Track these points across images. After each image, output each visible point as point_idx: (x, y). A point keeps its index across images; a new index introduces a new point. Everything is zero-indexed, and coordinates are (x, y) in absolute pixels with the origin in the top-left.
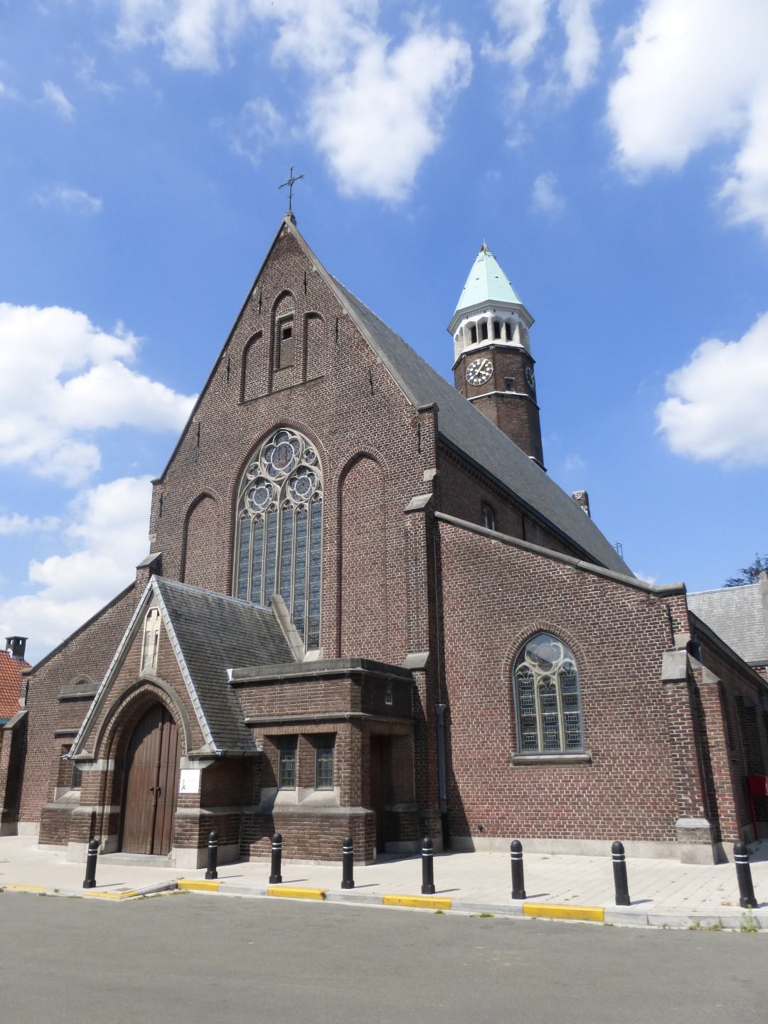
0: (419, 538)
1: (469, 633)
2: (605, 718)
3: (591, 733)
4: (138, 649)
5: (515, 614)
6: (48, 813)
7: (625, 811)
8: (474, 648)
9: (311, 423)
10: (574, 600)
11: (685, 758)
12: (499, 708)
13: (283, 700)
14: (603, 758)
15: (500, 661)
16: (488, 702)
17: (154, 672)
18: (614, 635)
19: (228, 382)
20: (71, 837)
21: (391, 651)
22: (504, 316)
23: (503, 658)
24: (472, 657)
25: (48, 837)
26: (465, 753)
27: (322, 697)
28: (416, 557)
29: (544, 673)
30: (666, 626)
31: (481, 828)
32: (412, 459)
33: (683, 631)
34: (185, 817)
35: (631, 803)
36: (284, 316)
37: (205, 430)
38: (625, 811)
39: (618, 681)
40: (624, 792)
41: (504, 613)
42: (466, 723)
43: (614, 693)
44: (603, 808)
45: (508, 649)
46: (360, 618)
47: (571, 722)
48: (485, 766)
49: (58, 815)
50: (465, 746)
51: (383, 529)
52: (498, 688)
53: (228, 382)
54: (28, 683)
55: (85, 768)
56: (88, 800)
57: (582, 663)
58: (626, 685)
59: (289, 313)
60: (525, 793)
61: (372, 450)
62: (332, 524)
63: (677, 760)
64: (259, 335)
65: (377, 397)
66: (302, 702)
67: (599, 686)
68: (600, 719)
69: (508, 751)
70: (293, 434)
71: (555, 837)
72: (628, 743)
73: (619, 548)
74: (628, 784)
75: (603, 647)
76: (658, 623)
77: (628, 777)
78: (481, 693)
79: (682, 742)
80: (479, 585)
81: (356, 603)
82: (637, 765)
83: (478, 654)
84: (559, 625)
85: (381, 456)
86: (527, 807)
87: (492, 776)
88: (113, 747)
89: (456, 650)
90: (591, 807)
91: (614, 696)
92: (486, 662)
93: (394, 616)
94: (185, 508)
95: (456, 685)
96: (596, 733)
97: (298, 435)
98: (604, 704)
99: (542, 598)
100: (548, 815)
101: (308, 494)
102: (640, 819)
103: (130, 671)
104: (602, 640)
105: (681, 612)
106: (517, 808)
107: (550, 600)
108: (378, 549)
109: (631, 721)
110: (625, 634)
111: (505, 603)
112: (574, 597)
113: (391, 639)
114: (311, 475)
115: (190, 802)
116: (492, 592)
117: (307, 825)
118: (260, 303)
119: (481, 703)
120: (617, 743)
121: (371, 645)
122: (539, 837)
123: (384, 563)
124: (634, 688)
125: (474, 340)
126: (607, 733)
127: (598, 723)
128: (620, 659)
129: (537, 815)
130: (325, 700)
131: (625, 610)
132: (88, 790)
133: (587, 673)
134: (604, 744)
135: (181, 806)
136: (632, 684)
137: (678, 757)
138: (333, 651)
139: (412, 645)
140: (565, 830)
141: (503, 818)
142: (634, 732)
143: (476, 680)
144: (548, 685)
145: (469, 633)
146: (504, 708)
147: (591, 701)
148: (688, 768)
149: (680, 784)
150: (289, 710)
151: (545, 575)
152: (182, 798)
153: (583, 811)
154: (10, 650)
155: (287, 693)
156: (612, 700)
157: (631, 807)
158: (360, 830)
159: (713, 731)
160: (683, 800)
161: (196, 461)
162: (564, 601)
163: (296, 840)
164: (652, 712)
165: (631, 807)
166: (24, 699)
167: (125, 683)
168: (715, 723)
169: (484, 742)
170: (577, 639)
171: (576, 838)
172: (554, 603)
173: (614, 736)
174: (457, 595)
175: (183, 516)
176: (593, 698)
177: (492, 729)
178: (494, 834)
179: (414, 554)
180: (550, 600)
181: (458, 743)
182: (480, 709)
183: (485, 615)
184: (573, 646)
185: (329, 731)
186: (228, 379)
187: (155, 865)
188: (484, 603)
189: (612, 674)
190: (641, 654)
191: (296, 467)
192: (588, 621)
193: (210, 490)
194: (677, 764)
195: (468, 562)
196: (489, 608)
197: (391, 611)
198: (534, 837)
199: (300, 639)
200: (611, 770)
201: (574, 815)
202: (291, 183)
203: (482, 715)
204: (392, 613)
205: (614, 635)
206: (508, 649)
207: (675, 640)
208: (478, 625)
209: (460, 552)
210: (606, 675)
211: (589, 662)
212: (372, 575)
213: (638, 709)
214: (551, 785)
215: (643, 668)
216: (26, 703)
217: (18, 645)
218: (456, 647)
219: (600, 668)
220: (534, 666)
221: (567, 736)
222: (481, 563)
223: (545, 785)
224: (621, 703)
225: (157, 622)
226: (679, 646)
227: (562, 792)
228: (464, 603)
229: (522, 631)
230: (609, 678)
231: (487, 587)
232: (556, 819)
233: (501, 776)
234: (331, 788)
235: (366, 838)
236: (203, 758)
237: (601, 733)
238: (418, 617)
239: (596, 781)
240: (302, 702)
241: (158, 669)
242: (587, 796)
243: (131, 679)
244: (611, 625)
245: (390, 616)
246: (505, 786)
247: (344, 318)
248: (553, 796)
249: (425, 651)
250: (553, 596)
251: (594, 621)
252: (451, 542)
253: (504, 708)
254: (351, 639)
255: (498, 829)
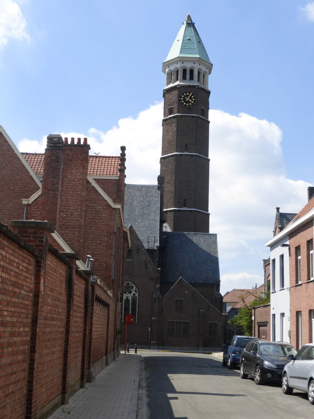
22: (188, 66)
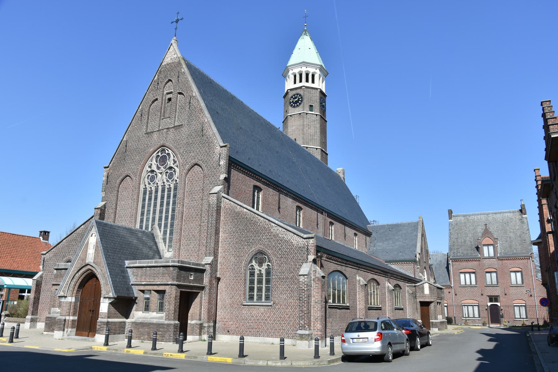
0: (214, 206)
1: (232, 249)
2: (279, 289)
3: (273, 295)
4: (86, 250)
5: (250, 243)
6: (48, 319)
7: (282, 326)
8: (233, 256)
9: (175, 147)
10: (273, 238)
11: (303, 306)
12: (240, 282)
13: (146, 275)
14: (277, 305)
15: (242, 262)
16: (236, 279)
17: (92, 261)
18: (286, 254)
19: (141, 122)
20: (56, 329)
21: (200, 255)
23: (243, 261)
24: (232, 260)
25: (49, 329)
26: (225, 300)
27: (161, 275)
28: (212, 214)
29: (259, 268)
30: (306, 252)
31: (228, 332)
32: (216, 169)
33: (312, 255)
34: (101, 322)
35: (285, 324)
36: (169, 91)
37: (129, 144)
38: (282, 326)
39: (286, 274)
40: (283, 319)
41: (246, 241)
42: (227, 288)
43: (284, 278)
44: (274, 325)
45: (246, 257)
46: (189, 239)
47: (268, 289)
48: (232, 306)
49: (53, 319)
50: (226, 297)
51: (202, 200)
52: (240, 274)
53: (141, 122)
54: (44, 259)
55: (63, 300)
56: (63, 314)
57: (273, 265)
58: (288, 275)
59: (171, 91)
60: (246, 318)
61: (200, 163)
62: (181, 195)
63: (301, 307)
64: (157, 99)
65: (205, 138)
66: (153, 277)
67: (278, 275)
68: (277, 289)
69: (242, 300)
70: (168, 151)
71: (256, 336)
72: (286, 299)
73: (358, 198)
74: (284, 316)
75: (282, 259)
76: (303, 250)
77: (285, 313)
78: (234, 275)
79: (303, 300)
80: (237, 229)
81: (188, 232)
82: (289, 308)
83: (234, 258)
84: (266, 248)
85: (203, 166)
86: (246, 324)
87: (235, 310)
88: (74, 292)
89: (226, 256)
90: (270, 324)
91: (283, 280)
92: (237, 262)
93: (203, 239)
94: (118, 181)
95: (224, 271)
96: (275, 295)
97: (170, 152)
98: (279, 283)
99: (261, 236)
100: (254, 327)
101: (172, 180)
102: (287, 330)
103: (83, 260)
104: (282, 256)
105: (312, 247)
106: (243, 324)
107: (264, 237)
108: (199, 209)
109: (288, 290)
110: (290, 254)
111: (247, 237)
112: (274, 237)
113: (200, 249)
114: (174, 171)
115: (103, 316)
116: (242, 232)
117: (151, 327)
118: (158, 84)
119: (234, 279)
120: (282, 299)
121: (193, 251)
122: (250, 336)
123: (201, 215)
124: (291, 277)
125: (295, 83)
126: (279, 295)
127: (276, 290)
128: (287, 265)
129: (250, 327)
130: (162, 277)
131: (292, 244)
132: (63, 309)
133: (275, 270)
134: (278, 299)
135: (100, 318)
136: (291, 275)
137: (301, 306)
138: (177, 253)
139: (207, 253)
140: (260, 333)
141: (237, 328)
142: (289, 295)
143: (232, 270)
144: (260, 273)
145: (232, 249)
146: (242, 282)
147: (275, 281)
148: (304, 310)
149: (300, 317)
150: (148, 280)
151: (263, 226)
152: (100, 314)
153: (267, 326)
154: (41, 238)
155: (148, 272)
156: (283, 281)
157: (284, 325)
158: (172, 330)
159: (317, 296)
160: (300, 323)
161: (124, 159)
162: (269, 238)
163: (147, 333)
164: (296, 287)
165: (284, 325)
166: (42, 266)
167: (80, 265)
168: (319, 293)
169: (233, 296)
170: (273, 255)
171: (264, 337)
172: (265, 239)
173: (282, 296)
174: (228, 232)
175: (117, 185)
176: (276, 280)
177: (236, 291)
178: (233, 334)
179: (211, 213)
180: (264, 237)
181: (223, 296)
182: (233, 282)
183: (238, 242)
184: (271, 258)
185: (163, 289)
186: (141, 120)
187: (89, 341)
188: (239, 236)
189: (284, 271)
190: (295, 263)
191: (168, 166)
192: (277, 248)
193: (130, 174)
194: (300, 309)
195: (234, 218)
196: (240, 239)
197: (202, 237)
198: (248, 336)
199: (164, 246)
200: (279, 310)
201: (264, 327)
202: (177, 21)
203: (233, 285)
204: (202, 238)
205: (286, 254)
206: (246, 257)
207: (308, 258)
208: (235, 246)
209: (231, 213)
210: (282, 271)
211: (276, 265)
212: (196, 220)
213: (291, 286)
214: (256, 315)
215: (295, 269)
216: (43, 268)
217: (45, 234)
218: (226, 255)
219: (280, 268)
220: (256, 265)
221: (265, 295)
222: (239, 219)
223: (254, 315)
224: (286, 283)
225: (93, 239)
226: (310, 261)
227: (260, 318)
228: (231, 236)
229: (252, 250)
230: (283, 272)
231: (240, 230)
232: (257, 329)
233: (238, 310)
234: (163, 313)
235: (174, 333)
236: (110, 298)
237: (277, 295)
238: (210, 241)
239: (273, 314)
240: (153, 277)
241: (94, 260)
242: (269, 320)
243: (83, 263)
244: (286, 250)
245: (201, 239)
246: (239, 315)
247: (194, 97)
248: (257, 320)
249: (212, 256)
250: (265, 236)
251: (280, 248)
252: (228, 208)
253: (242, 282)
254: (185, 248)
255: (235, 332)
